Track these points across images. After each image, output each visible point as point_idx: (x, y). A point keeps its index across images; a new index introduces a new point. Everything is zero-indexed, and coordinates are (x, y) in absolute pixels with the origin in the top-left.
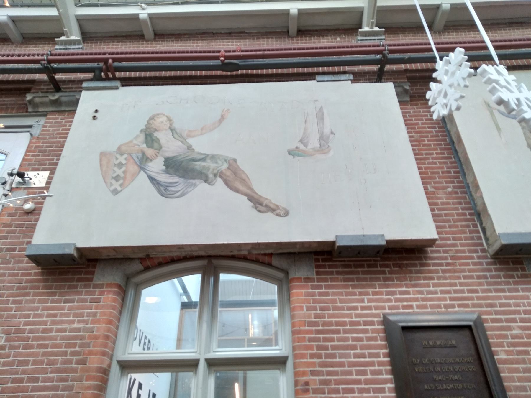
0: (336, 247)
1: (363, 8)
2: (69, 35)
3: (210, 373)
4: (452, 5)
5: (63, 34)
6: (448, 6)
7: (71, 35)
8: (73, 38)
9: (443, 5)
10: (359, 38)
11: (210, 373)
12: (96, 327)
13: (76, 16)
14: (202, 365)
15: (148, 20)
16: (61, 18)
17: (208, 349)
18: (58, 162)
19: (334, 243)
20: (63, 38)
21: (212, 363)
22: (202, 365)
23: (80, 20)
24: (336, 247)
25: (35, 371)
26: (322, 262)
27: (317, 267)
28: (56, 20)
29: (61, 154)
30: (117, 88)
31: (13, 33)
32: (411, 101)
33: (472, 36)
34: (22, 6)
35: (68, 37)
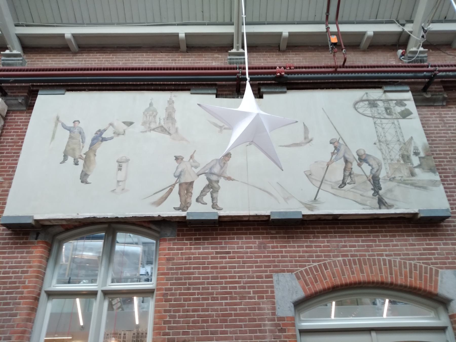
0: (271, 219)
1: (233, 33)
2: (12, 49)
3: (105, 298)
4: (289, 33)
5: (7, 48)
6: (184, 35)
7: (14, 49)
8: (15, 52)
9: (66, 35)
10: (229, 57)
11: (105, 298)
12: (33, 260)
13: (16, 34)
14: (100, 294)
15: (73, 40)
16: (3, 35)
17: (105, 283)
18: (22, 145)
19: (269, 216)
20: (7, 52)
21: (106, 293)
22: (100, 294)
23: (20, 38)
24: (271, 219)
25: (10, 288)
26: (262, 230)
27: (179, 231)
28: (231, 36)
29: (24, 138)
30: (285, 92)
31: (74, 45)
32: (28, 110)
33: (307, 61)
34: (209, 24)
35: (11, 51)
